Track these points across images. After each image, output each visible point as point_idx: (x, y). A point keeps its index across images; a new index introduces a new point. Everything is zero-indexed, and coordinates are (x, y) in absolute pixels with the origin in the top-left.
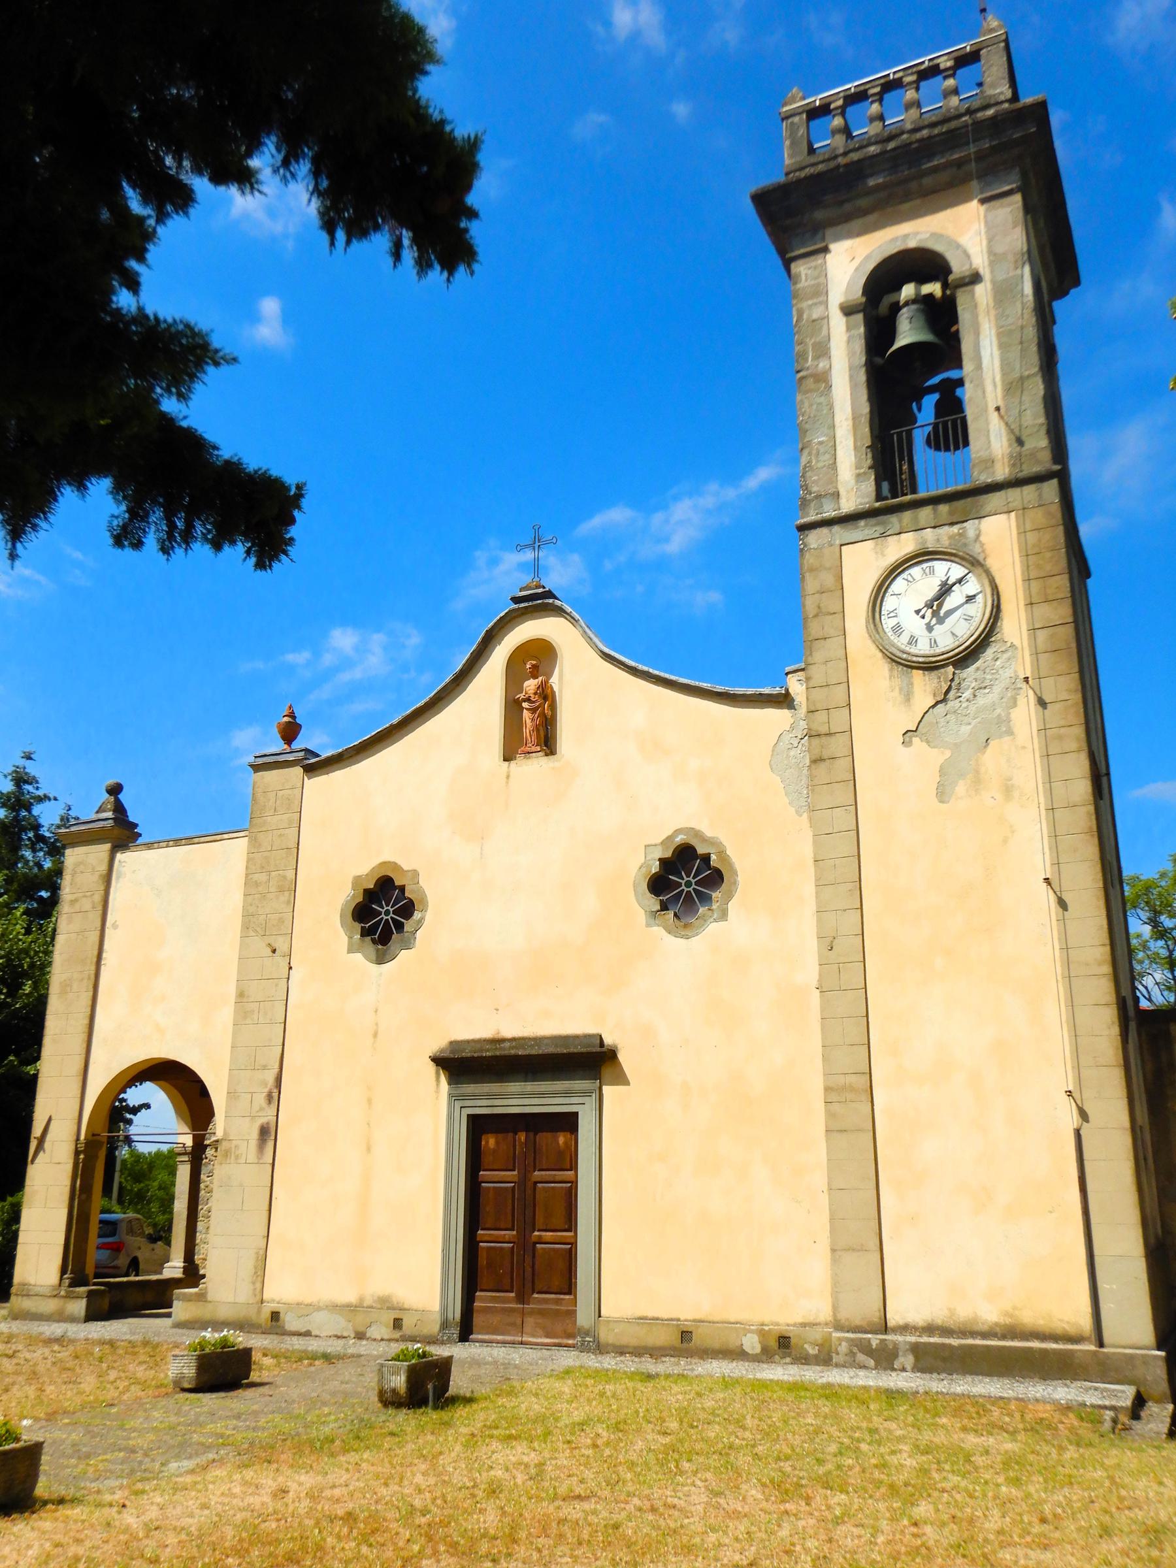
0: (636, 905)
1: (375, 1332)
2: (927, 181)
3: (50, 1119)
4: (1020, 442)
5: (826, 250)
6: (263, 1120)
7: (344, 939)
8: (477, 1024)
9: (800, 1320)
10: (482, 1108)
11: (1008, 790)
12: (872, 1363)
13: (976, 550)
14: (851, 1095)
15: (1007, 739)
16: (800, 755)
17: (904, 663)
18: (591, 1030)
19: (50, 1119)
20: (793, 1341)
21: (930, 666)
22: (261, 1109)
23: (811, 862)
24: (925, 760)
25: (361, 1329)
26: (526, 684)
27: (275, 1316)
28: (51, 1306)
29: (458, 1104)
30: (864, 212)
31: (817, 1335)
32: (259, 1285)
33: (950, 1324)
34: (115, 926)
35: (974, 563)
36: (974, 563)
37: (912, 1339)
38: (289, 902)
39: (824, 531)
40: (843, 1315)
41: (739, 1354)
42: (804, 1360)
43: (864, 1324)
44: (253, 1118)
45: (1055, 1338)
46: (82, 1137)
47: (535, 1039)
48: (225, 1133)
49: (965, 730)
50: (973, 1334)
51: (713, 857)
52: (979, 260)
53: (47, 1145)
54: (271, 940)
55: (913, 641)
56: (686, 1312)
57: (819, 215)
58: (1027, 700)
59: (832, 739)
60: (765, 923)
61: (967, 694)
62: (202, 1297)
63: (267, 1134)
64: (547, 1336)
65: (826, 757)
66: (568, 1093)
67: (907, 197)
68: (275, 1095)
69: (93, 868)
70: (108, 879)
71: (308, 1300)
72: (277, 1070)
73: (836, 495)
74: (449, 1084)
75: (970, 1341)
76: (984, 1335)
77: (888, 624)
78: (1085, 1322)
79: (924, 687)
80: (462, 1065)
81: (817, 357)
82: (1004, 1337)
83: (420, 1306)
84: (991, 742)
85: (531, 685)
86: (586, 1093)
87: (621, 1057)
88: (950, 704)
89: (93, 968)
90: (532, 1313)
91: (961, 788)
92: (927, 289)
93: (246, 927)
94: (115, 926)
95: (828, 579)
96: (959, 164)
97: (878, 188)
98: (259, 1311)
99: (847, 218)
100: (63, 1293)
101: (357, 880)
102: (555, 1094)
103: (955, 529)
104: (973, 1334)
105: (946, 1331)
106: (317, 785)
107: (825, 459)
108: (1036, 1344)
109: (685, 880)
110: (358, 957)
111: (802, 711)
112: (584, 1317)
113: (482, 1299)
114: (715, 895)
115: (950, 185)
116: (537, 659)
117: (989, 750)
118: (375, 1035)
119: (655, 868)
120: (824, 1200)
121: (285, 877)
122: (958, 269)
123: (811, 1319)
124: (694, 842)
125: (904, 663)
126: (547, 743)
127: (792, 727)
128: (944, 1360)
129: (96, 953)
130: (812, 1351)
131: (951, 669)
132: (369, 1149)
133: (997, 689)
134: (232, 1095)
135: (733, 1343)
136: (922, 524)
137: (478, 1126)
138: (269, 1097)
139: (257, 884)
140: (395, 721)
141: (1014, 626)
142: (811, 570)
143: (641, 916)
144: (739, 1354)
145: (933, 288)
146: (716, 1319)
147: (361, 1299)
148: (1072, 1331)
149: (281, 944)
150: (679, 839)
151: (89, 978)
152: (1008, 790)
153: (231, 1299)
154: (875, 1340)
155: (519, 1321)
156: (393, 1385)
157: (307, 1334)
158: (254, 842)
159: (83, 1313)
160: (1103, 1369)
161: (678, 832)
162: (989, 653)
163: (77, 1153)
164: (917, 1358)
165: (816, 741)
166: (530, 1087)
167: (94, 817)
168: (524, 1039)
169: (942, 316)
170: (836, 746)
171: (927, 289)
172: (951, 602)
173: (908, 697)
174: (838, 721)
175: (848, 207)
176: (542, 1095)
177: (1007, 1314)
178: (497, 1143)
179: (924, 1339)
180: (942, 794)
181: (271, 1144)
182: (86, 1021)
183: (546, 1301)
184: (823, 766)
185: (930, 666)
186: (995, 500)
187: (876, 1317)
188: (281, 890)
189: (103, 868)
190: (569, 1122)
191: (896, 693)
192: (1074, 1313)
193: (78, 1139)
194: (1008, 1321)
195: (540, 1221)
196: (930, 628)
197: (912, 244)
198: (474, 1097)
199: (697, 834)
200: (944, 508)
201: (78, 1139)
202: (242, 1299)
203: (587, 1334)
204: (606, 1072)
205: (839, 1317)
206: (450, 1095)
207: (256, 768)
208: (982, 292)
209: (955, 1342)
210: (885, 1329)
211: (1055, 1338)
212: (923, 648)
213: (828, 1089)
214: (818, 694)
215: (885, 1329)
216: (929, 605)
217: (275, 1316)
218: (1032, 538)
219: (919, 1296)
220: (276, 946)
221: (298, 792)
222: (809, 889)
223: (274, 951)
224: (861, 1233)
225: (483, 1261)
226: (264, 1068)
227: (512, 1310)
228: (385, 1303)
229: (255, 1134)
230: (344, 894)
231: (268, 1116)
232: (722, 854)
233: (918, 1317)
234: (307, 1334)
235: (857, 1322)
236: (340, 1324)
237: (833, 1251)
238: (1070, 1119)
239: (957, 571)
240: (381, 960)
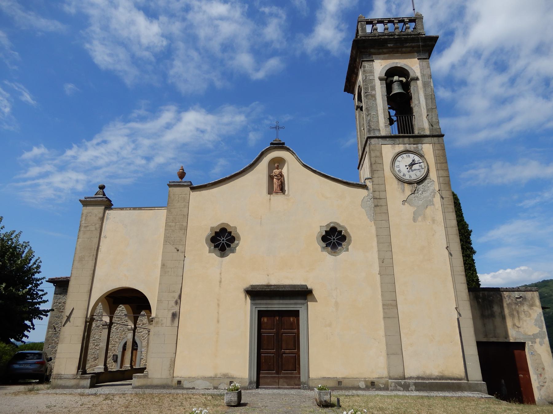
0: (317, 246)
1: (222, 386)
2: (404, 49)
3: (73, 309)
4: (432, 126)
5: (373, 61)
6: (174, 311)
7: (207, 248)
8: (260, 280)
9: (377, 376)
10: (263, 308)
11: (434, 221)
12: (402, 389)
13: (422, 152)
14: (390, 307)
15: (433, 206)
16: (371, 203)
17: (401, 181)
18: (303, 283)
19: (73, 309)
20: (376, 383)
21: (410, 183)
22: (173, 307)
23: (375, 236)
24: (408, 210)
25: (216, 386)
26: (274, 171)
27: (179, 382)
28: (73, 382)
29: (254, 307)
30: (385, 53)
31: (383, 381)
32: (172, 371)
33: (424, 376)
34: (105, 237)
35: (421, 156)
36: (421, 156)
37: (414, 381)
38: (184, 234)
39: (376, 139)
40: (391, 375)
41: (359, 388)
42: (380, 389)
43: (398, 377)
44: (169, 310)
45: (454, 379)
46: (89, 316)
47: (283, 285)
48: (156, 315)
49: (420, 202)
50: (431, 379)
51: (343, 232)
52: (418, 74)
53: (71, 319)
54: (177, 246)
55: (404, 175)
56: (339, 375)
57: (372, 50)
58: (438, 197)
59: (381, 200)
60: (361, 252)
61: (420, 192)
62: (146, 376)
63: (175, 316)
64: (288, 385)
65: (378, 205)
66: (296, 304)
67: (397, 52)
68: (179, 302)
69: (96, 215)
70: (102, 219)
71: (194, 376)
72: (179, 293)
73: (379, 130)
74: (251, 300)
75: (430, 381)
76: (434, 379)
77: (397, 169)
78: (463, 374)
79: (408, 189)
80: (255, 293)
81: (372, 90)
82: (440, 379)
83: (240, 377)
84: (428, 207)
85: (276, 171)
86: (303, 304)
87: (314, 292)
88: (416, 195)
89: (95, 252)
90: (282, 378)
91: (420, 219)
92: (401, 79)
93: (166, 241)
94: (105, 237)
95: (378, 154)
96: (413, 47)
97: (391, 48)
98: (172, 381)
99: (379, 54)
100: (78, 377)
101: (212, 229)
102: (291, 304)
103: (415, 146)
104: (431, 379)
105: (423, 378)
106: (195, 196)
107: (375, 120)
108: (449, 381)
109: (334, 238)
110: (213, 255)
111: (371, 191)
112: (303, 379)
113: (263, 374)
114: (343, 243)
115: (410, 52)
116: (279, 163)
117: (428, 209)
118: (220, 282)
119: (324, 233)
120: (384, 339)
121: (183, 225)
122: (412, 75)
123: (381, 376)
124: (336, 226)
125: (401, 181)
126: (282, 189)
127: (368, 195)
128: (424, 387)
129: (97, 246)
130: (382, 386)
131: (416, 184)
132: (218, 322)
133: (429, 192)
134: (159, 301)
135: (356, 384)
136: (406, 143)
137: (261, 314)
138: (176, 303)
139: (170, 226)
140: (228, 176)
141: (433, 175)
142: (373, 150)
143: (320, 249)
144: (359, 388)
145: (404, 80)
146: (350, 377)
147: (216, 375)
148: (459, 377)
149: (180, 248)
150: (332, 225)
151: (93, 255)
152: (434, 221)
153: (159, 377)
154: (403, 382)
155: (277, 381)
156: (325, 399)
157: (194, 388)
158: (169, 211)
159: (89, 385)
160: (471, 388)
161: (331, 223)
162: (426, 182)
163: (86, 322)
164: (416, 387)
165: (375, 200)
166: (281, 301)
167: (94, 196)
168: (279, 285)
169: (406, 86)
170: (382, 202)
171: (401, 79)
172: (415, 167)
173: (403, 191)
174: (382, 195)
175: (381, 50)
176: (287, 304)
177: (440, 372)
178: (267, 320)
179: (417, 381)
180: (415, 220)
181: (177, 319)
182: (92, 272)
183: (287, 373)
184: (378, 208)
185: (410, 183)
186: (426, 140)
187: (401, 375)
188: (181, 229)
189: (101, 215)
190: (296, 314)
191: (400, 189)
192: (459, 371)
193: (87, 317)
194: (441, 374)
195: (284, 346)
196: (409, 172)
197: (399, 65)
198: (260, 304)
199: (338, 224)
200: (411, 139)
201: (87, 317)
202: (164, 377)
203: (305, 384)
204: (309, 297)
205: (390, 375)
206: (252, 304)
207: (170, 186)
208: (419, 83)
209: (427, 382)
210: (405, 379)
211: (454, 379)
212: (407, 177)
213: (383, 305)
214: (375, 186)
215: (405, 379)
216: (409, 166)
217: (179, 382)
218: (437, 152)
219: (414, 368)
220: (179, 249)
221: (188, 196)
222: (375, 244)
223: (178, 251)
224: (395, 349)
225: (263, 360)
226: (174, 292)
227: (275, 377)
228: (226, 376)
229: (170, 316)
230: (207, 233)
231: (176, 309)
232: (346, 231)
233: (414, 375)
234: (194, 388)
235: (396, 377)
236: (208, 384)
237: (388, 354)
238: (456, 316)
239: (417, 159)
240: (222, 256)
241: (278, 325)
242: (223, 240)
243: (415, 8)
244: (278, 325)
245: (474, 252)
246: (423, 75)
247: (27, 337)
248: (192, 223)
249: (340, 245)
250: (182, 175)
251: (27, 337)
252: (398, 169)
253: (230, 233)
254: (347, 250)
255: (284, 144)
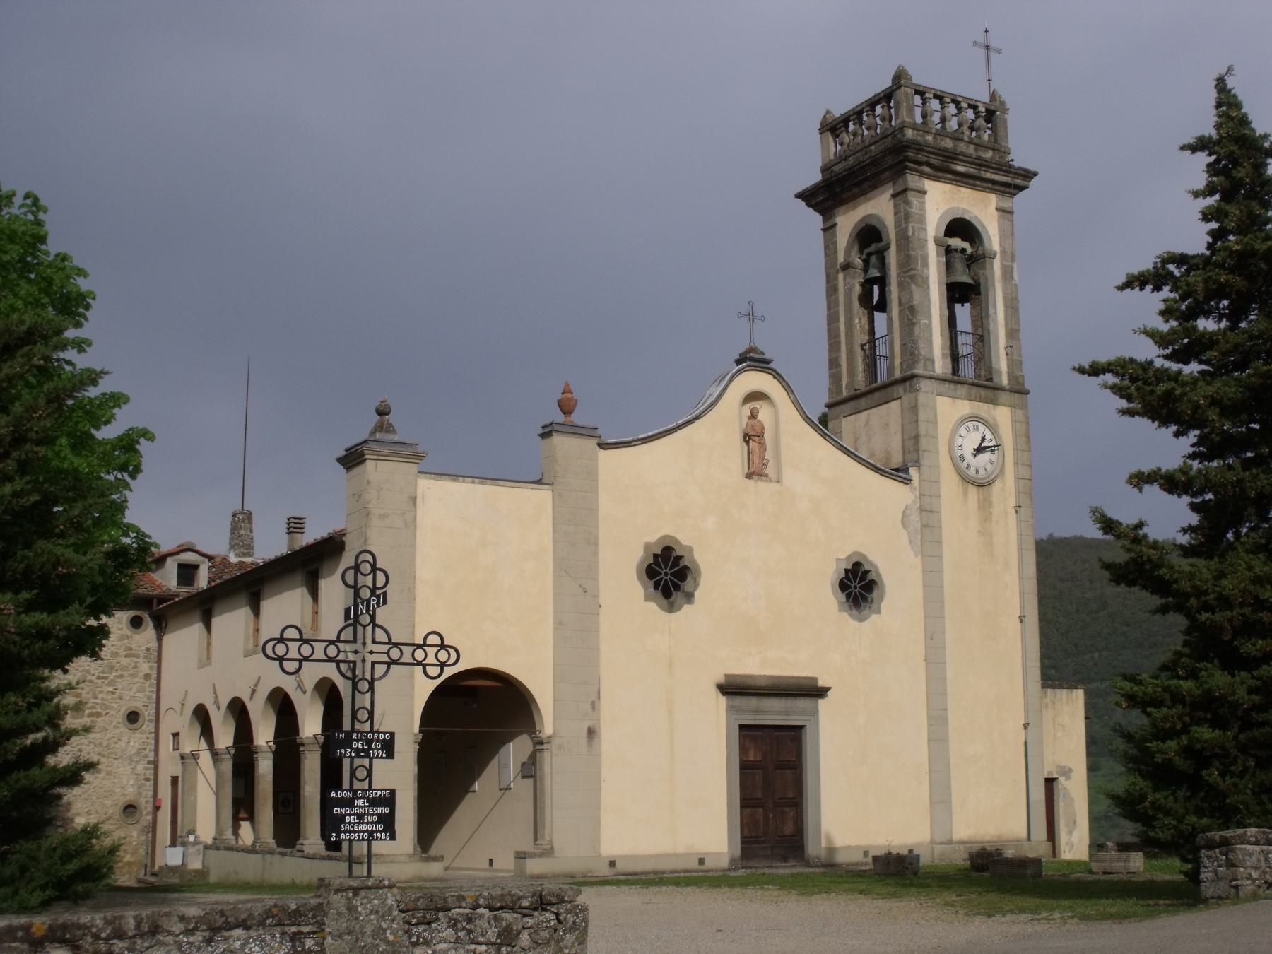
63: (591, 733)
101: (647, 546)
106: (602, 453)
119: (843, 575)
197: (967, 217)
224: (941, 799)
229: (585, 732)
240: (671, 608)
241: (772, 763)
242: (666, 574)
243: (993, 77)
244: (772, 763)
245: (1159, 469)
246: (1003, 252)
247: (81, 345)
248: (605, 533)
249: (656, 587)
250: (566, 407)
251: (81, 345)
252: (960, 453)
253: (679, 558)
254: (647, 599)
255: (768, 362)
